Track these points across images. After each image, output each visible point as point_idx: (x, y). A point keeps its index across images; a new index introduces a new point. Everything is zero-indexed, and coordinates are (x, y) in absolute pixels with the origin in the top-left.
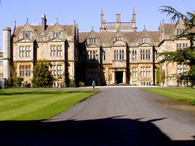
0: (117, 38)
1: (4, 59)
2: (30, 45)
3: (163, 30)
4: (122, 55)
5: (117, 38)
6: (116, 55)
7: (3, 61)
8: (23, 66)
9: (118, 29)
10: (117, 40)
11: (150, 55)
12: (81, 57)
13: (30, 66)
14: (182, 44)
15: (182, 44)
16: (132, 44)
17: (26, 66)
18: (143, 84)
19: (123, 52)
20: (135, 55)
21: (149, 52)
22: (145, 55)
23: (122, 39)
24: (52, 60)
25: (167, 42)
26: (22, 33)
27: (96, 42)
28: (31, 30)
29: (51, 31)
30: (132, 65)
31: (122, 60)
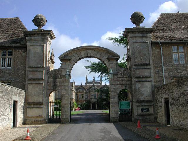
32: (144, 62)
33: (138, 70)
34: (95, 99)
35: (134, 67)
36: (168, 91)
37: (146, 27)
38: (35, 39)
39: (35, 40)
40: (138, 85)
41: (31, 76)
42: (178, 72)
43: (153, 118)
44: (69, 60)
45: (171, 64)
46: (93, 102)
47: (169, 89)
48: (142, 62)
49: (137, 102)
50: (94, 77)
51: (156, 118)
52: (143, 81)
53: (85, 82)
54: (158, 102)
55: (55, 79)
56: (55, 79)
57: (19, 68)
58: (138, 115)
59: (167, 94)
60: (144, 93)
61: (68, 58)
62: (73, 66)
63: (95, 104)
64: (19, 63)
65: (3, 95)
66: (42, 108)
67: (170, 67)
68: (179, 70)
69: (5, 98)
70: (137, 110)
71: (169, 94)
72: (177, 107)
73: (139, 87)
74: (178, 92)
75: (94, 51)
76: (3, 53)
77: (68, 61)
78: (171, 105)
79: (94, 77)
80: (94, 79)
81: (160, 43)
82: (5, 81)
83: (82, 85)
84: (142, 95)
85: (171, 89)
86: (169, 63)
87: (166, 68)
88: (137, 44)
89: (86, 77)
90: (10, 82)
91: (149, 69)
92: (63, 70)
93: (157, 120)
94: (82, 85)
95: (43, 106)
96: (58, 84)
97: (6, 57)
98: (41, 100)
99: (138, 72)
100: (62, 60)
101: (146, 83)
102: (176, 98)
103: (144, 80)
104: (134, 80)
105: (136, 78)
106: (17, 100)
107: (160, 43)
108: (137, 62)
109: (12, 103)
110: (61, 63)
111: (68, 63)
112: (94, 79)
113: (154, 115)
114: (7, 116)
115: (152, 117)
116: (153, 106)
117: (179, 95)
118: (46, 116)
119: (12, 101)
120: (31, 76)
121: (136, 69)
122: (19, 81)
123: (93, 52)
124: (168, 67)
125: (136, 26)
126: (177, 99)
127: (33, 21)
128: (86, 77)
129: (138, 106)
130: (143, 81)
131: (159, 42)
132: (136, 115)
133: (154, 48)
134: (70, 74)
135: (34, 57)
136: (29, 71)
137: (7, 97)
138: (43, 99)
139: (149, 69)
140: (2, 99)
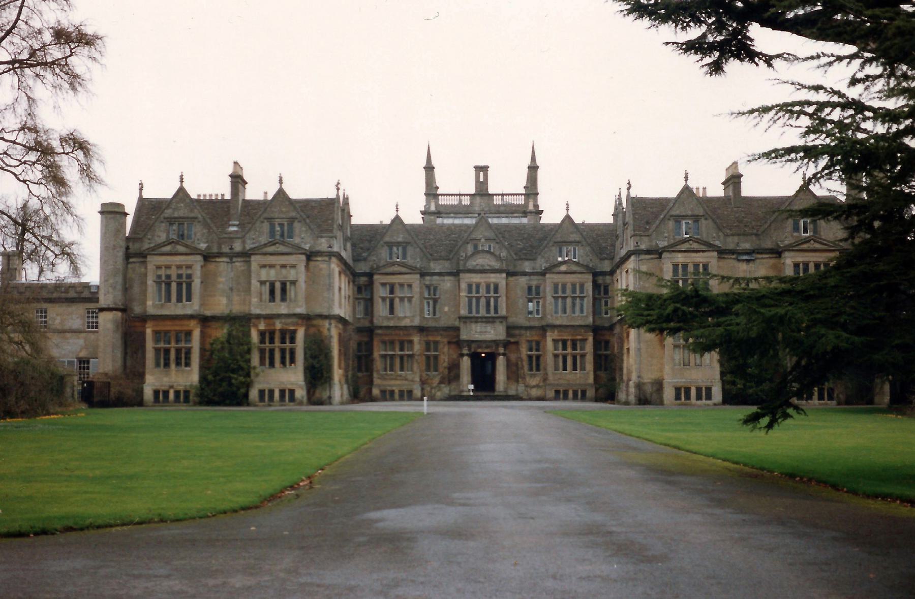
0: (476, 246)
1: (102, 310)
2: (189, 263)
3: (627, 220)
4: (492, 300)
5: (476, 246)
6: (474, 300)
7: (97, 317)
8: (167, 332)
9: (479, 214)
10: (476, 252)
11: (500, 299)
12: (428, 303)
13: (189, 334)
14: (569, 287)
15: (569, 287)
16: (527, 263)
17: (178, 333)
18: (561, 396)
19: (496, 291)
20: (535, 301)
21: (582, 291)
22: (483, 301)
23: (494, 248)
24: (264, 313)
25: (642, 257)
26: (163, 224)
27: (409, 258)
28: (192, 215)
29: (262, 219)
30: (523, 332)
31: (493, 318)
50: (482, 169)
53: (421, 202)
79: (482, 169)
83: (397, 220)
89: (429, 169)
94: (397, 220)
128: (429, 169)
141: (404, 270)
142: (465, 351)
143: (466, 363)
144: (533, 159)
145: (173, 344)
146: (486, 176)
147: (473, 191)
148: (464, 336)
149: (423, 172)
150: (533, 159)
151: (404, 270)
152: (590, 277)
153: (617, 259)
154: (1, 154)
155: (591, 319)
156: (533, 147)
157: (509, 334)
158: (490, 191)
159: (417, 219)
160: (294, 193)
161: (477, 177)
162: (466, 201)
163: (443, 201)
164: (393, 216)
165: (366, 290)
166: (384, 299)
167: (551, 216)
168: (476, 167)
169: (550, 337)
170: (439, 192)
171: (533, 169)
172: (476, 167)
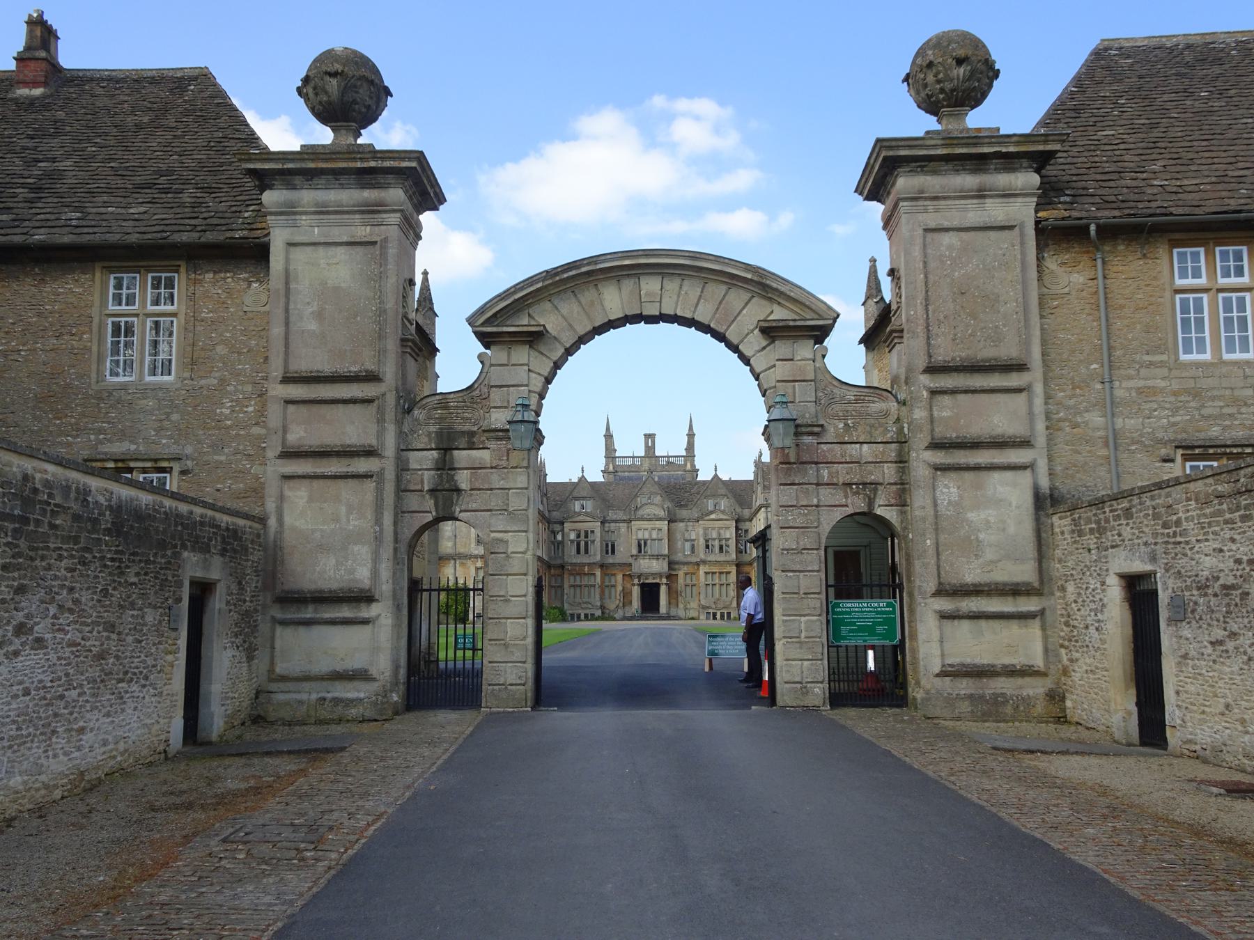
32: (986, 352)
33: (946, 400)
34: (657, 557)
35: (925, 379)
36: (1155, 535)
37: (1002, 132)
38: (317, 205)
39: (322, 211)
40: (949, 489)
41: (298, 435)
42: (1205, 412)
43: (1041, 691)
44: (534, 338)
45: (1162, 364)
46: (647, 576)
47: (1156, 516)
48: (970, 352)
49: (942, 591)
50: (650, 437)
51: (1056, 697)
52: (977, 468)
53: (601, 463)
54: (1071, 596)
55: (447, 444)
56: (447, 444)
57: (222, 381)
58: (943, 674)
59: (1143, 548)
60: (982, 536)
61: (523, 322)
62: (555, 374)
63: (658, 586)
64: (221, 350)
65: (122, 552)
66: (365, 622)
67: (1150, 383)
68: (1213, 398)
69: (135, 569)
70: (941, 641)
71: (1160, 549)
72: (1219, 633)
73: (950, 502)
74: (1233, 540)
75: (677, 281)
76: (119, 286)
77: (524, 343)
78: (1172, 621)
79: (650, 437)
80: (650, 449)
81: (1093, 228)
82: (136, 460)
83: (582, 479)
84: (971, 546)
85: (1178, 523)
86: (1146, 358)
87: (1131, 384)
88: (947, 239)
89: (609, 437)
90: (165, 464)
91: (1019, 390)
92: (496, 397)
93: (1069, 704)
94: (582, 479)
95: (374, 610)
96: (463, 479)
97: (137, 315)
98: (362, 576)
99: (946, 408)
100: (486, 339)
101: (996, 476)
102: (1218, 578)
103: (983, 457)
104: (922, 459)
105: (936, 445)
106: (214, 575)
107: (1093, 228)
108: (945, 351)
109: (179, 600)
110: (481, 358)
111: (521, 354)
112: (650, 449)
113: (1044, 674)
114: (146, 678)
115: (1035, 689)
116: (1038, 619)
117: (1238, 561)
118: (388, 674)
119: (179, 584)
120: (302, 434)
121: (934, 392)
122: (223, 458)
123: (672, 285)
124: (1141, 383)
125: (938, 127)
126: (1224, 587)
127: (299, 91)
128: (609, 437)
129: (944, 616)
130: (977, 468)
131: (1088, 226)
132: (937, 670)
133: (1051, 263)
134: (536, 423)
135: (319, 315)
136: (289, 402)
137: (148, 562)
138: (375, 574)
139: (1019, 390)
140: (110, 574)
141: (588, 519)
142: (636, 581)
143: (636, 591)
144: (608, 429)
145: (122, 339)
146: (653, 442)
147: (643, 454)
148: (635, 569)
149: (686, 438)
150: (608, 429)
151: (588, 519)
152: (734, 523)
153: (754, 508)
154: (1253, 404)
155: (734, 556)
156: (608, 423)
157: (670, 568)
158: (657, 454)
159: (599, 478)
160: (724, 477)
161: (646, 443)
162: (638, 462)
163: (619, 462)
164: (580, 476)
165: (674, 570)
166: (572, 542)
167: (704, 475)
168: (645, 435)
169: (703, 569)
170: (617, 455)
171: (691, 436)
172: (645, 435)
